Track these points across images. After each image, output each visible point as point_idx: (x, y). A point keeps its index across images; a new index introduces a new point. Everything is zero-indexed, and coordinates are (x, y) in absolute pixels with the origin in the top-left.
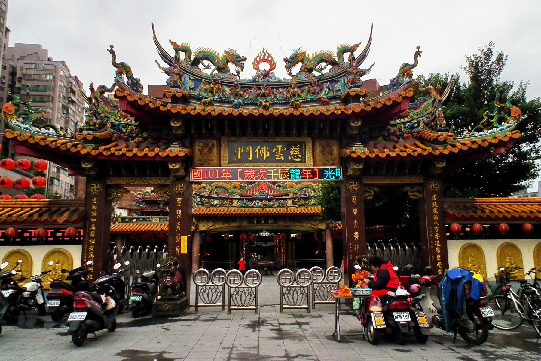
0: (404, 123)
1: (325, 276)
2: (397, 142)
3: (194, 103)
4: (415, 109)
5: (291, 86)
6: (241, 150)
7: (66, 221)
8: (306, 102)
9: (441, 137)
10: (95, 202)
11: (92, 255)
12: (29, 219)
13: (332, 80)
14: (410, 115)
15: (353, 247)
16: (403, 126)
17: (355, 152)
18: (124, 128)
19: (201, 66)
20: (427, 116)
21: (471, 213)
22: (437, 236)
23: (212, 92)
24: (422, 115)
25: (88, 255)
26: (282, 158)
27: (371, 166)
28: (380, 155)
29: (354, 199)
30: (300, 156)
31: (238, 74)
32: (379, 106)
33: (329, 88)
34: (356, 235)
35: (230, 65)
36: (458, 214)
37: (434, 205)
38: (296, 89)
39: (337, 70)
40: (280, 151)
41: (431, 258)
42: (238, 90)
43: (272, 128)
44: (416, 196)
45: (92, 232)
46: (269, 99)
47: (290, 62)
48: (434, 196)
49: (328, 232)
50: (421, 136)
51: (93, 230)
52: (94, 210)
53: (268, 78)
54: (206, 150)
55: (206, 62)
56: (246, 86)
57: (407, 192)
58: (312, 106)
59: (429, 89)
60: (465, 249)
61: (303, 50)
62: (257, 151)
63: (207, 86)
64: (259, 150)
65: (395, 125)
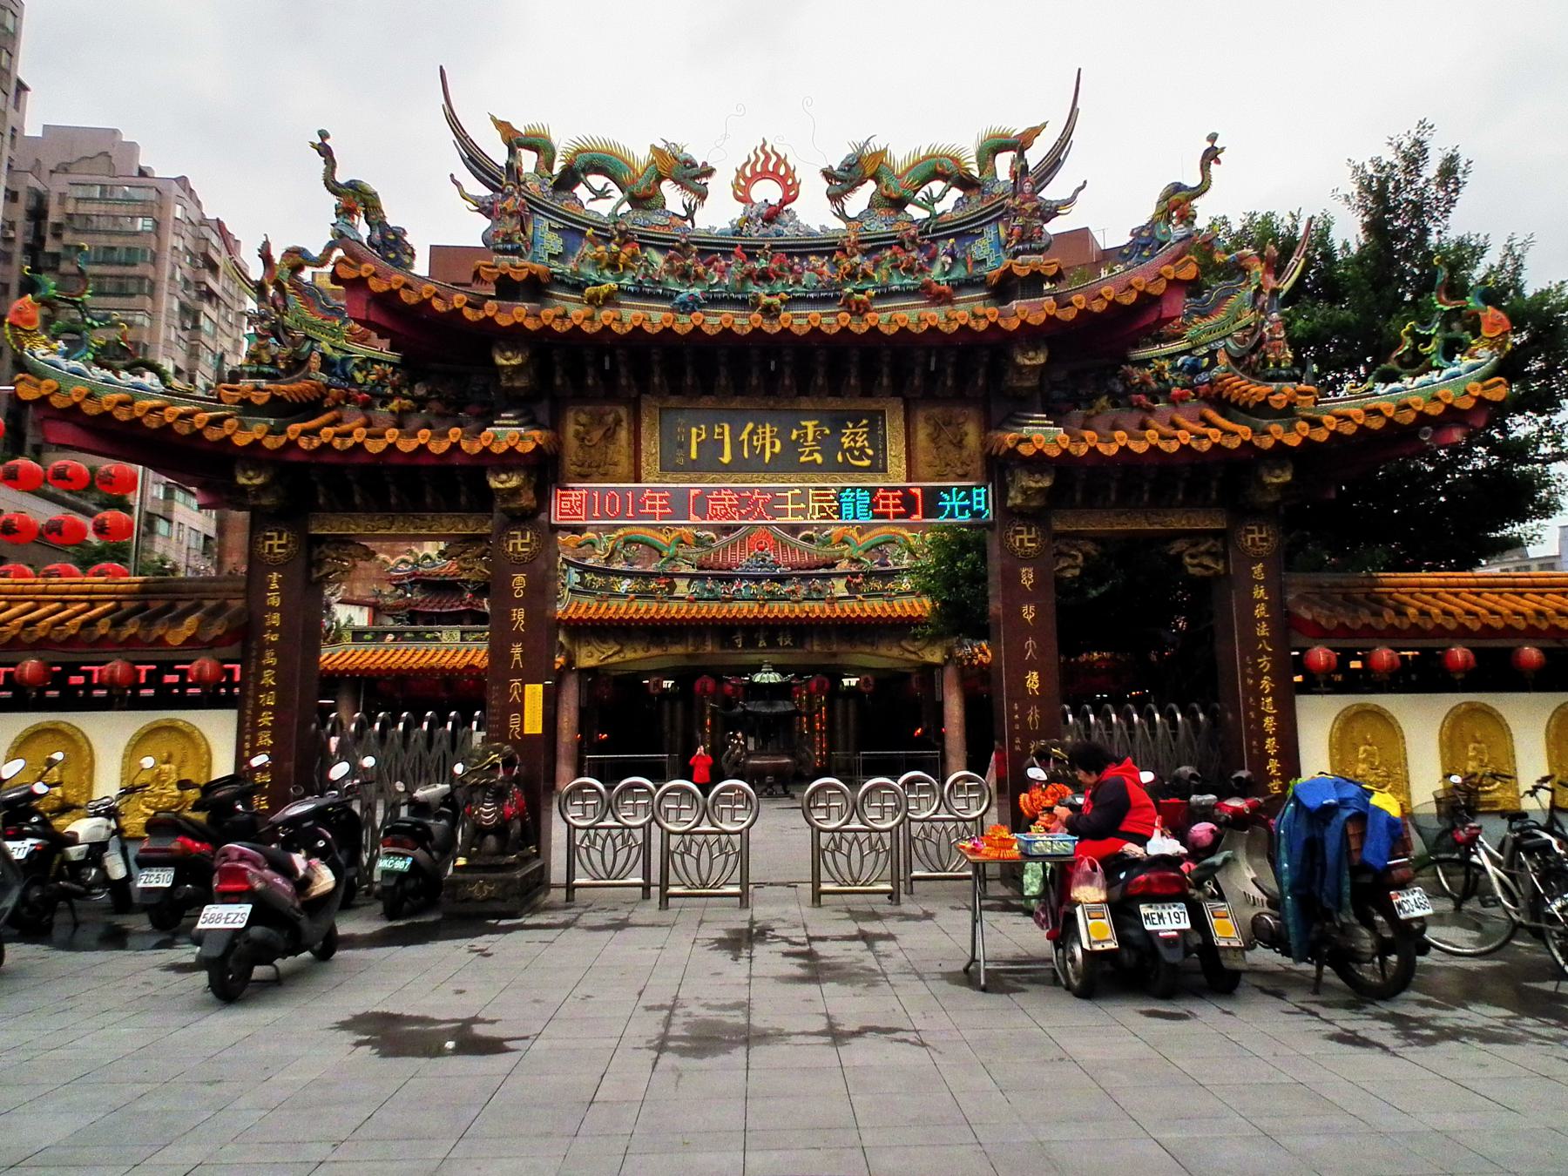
6: (699, 435)
13: (964, 231)
16: (1167, 365)
21: (1365, 617)
27: (1074, 480)
28: (1102, 448)
29: (1027, 577)
30: (870, 452)
33: (953, 256)
39: (977, 204)
40: (810, 437)
47: (842, 181)
48: (1258, 569)
49: (950, 672)
52: (273, 609)
57: (1179, 555)
59: (1242, 258)
61: (877, 145)
62: (745, 436)
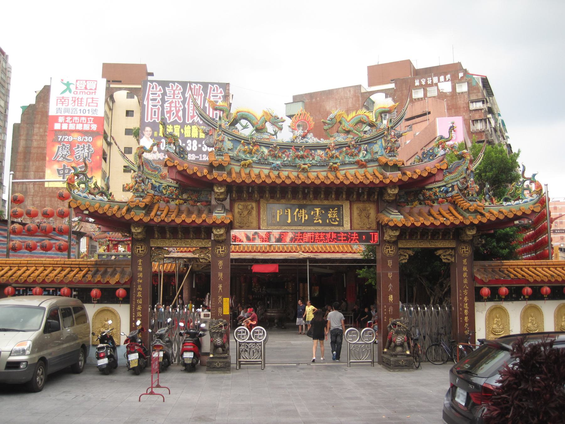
0: (439, 187)
1: (360, 337)
2: (432, 206)
3: (234, 165)
4: (450, 173)
5: (329, 148)
6: (280, 213)
7: (118, 283)
8: (344, 164)
9: (471, 207)
10: (140, 264)
11: (139, 314)
12: (83, 279)
13: (370, 142)
14: (446, 179)
15: (388, 309)
16: (438, 190)
17: (392, 220)
18: (165, 189)
19: (238, 126)
20: (461, 180)
22: (466, 299)
23: (250, 153)
24: (456, 179)
25: (136, 314)
26: (320, 221)
27: (407, 232)
28: (416, 224)
29: (390, 263)
30: (338, 219)
31: (276, 134)
32: (415, 177)
33: (366, 150)
34: (391, 298)
35: (268, 125)
36: (486, 278)
37: (465, 269)
38: (334, 152)
39: (374, 132)
40: (318, 214)
41: (460, 320)
42: (276, 152)
43: (311, 193)
44: (449, 260)
45: (139, 293)
46: (307, 161)
48: (465, 261)
50: (454, 202)
51: (139, 291)
52: (140, 272)
53: (306, 139)
54: (245, 213)
55: (244, 122)
56: (284, 147)
58: (351, 169)
59: (463, 153)
60: (491, 311)
62: (295, 213)
63: (246, 147)
64: (297, 213)
65: (431, 189)
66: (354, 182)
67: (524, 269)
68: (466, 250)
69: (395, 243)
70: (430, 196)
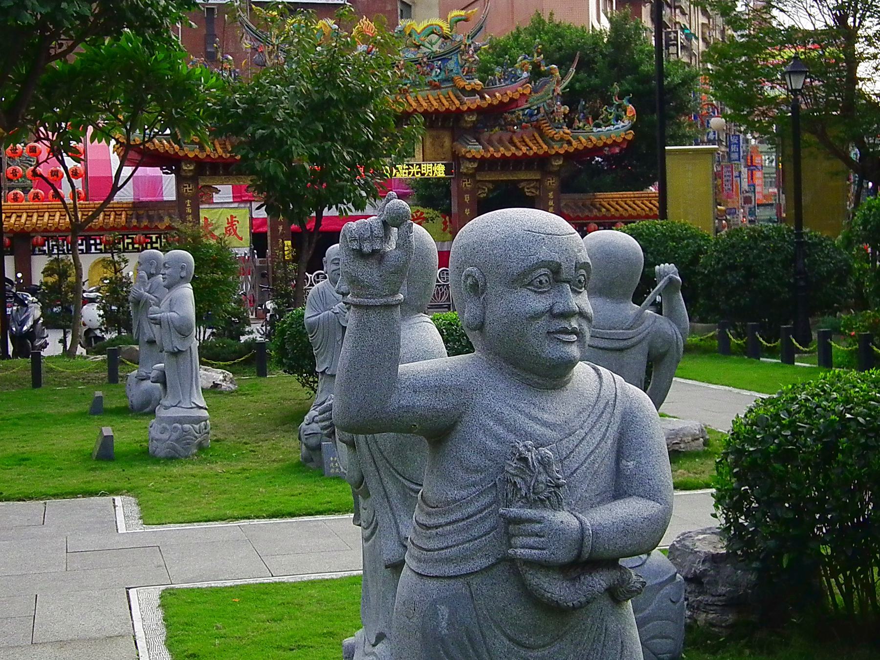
0: (523, 110)
13: (443, 58)
16: (521, 113)
21: (587, 213)
27: (485, 164)
28: (495, 154)
29: (467, 198)
33: (440, 68)
39: (449, 45)
48: (551, 195)
52: (189, 214)
57: (523, 188)
59: (551, 69)
66: (429, 109)
67: (620, 202)
68: (552, 182)
69: (472, 176)
70: (512, 120)
